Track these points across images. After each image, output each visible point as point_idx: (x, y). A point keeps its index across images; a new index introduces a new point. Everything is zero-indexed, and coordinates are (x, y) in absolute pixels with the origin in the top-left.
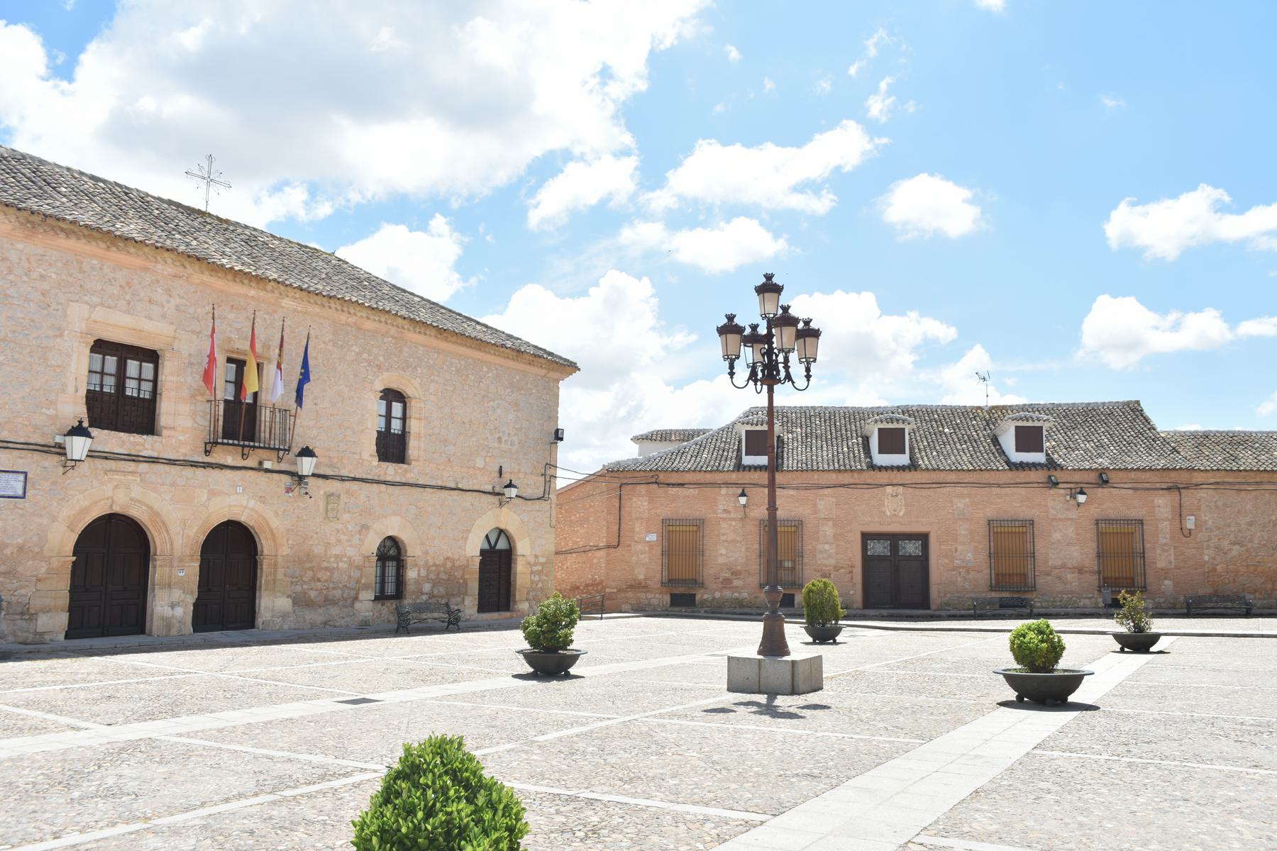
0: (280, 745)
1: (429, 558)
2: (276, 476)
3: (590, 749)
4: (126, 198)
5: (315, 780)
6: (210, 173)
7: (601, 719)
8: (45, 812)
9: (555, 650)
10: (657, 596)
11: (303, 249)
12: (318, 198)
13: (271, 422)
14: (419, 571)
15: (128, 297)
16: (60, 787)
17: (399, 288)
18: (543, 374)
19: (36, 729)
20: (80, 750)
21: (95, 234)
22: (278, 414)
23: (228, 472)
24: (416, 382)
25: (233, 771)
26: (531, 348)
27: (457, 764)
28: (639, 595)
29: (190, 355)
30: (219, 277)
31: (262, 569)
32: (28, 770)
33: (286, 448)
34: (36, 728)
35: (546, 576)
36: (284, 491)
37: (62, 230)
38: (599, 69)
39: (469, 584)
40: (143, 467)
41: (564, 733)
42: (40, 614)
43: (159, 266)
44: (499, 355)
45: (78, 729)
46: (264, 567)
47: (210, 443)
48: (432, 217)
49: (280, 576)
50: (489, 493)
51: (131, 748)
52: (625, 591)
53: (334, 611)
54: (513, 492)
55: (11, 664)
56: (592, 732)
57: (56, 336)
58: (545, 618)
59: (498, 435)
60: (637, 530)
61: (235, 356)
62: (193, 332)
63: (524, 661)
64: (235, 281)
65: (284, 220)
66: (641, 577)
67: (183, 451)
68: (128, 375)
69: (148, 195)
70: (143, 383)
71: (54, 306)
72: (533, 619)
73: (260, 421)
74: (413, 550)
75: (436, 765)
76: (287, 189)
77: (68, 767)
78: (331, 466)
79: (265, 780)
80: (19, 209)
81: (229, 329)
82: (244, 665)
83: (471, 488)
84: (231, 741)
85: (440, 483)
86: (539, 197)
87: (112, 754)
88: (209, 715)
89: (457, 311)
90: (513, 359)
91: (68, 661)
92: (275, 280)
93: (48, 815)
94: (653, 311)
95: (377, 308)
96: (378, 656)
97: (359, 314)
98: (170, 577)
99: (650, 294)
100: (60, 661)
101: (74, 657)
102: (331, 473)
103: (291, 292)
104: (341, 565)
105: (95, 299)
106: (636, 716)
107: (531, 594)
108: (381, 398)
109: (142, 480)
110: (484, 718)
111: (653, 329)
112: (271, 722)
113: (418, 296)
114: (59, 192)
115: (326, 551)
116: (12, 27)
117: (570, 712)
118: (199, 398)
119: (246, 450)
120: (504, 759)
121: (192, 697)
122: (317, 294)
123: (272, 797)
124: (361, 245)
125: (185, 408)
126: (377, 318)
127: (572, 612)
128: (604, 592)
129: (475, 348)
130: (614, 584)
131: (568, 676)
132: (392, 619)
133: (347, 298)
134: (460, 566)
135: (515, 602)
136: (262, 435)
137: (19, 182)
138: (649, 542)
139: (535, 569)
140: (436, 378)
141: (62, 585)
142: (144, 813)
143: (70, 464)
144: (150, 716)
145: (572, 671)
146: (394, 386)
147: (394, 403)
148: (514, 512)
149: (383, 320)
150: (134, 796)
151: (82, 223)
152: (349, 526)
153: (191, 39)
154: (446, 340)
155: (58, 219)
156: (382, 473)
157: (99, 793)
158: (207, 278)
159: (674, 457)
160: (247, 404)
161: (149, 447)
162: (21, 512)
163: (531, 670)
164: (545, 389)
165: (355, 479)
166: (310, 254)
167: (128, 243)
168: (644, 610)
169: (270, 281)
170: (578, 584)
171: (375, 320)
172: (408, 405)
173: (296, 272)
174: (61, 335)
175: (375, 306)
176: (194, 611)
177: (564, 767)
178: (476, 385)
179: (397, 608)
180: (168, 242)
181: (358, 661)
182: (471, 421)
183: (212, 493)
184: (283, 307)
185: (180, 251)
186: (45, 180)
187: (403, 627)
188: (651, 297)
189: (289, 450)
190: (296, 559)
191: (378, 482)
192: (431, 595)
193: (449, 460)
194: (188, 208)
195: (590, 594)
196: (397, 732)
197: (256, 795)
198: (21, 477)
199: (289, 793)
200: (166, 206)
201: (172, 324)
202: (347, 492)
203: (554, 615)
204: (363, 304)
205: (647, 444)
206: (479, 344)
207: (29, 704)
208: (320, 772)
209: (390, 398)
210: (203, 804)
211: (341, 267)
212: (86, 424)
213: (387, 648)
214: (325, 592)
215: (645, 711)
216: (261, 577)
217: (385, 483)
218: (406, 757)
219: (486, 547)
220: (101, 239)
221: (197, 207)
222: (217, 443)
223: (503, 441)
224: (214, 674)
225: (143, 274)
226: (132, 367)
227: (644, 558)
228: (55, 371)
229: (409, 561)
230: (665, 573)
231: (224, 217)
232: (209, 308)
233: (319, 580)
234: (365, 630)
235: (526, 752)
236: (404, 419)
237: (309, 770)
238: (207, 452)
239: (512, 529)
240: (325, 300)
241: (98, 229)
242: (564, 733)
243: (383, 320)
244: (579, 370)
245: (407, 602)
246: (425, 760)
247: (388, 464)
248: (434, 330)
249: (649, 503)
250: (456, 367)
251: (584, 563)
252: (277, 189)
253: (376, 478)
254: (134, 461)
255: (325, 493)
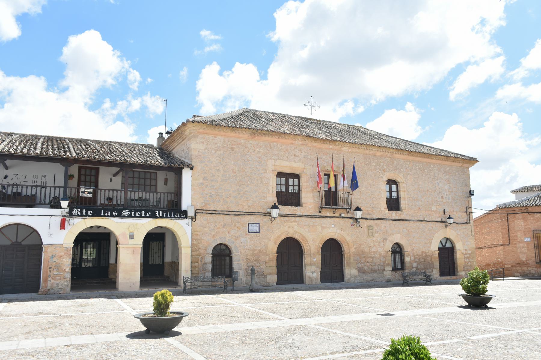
0: (354, 332)
1: (414, 252)
2: (346, 219)
3: (499, 345)
4: (284, 118)
5: (367, 348)
6: (312, 103)
7: (506, 331)
8: (267, 351)
9: (479, 295)
10: (534, 269)
11: (350, 126)
12: (358, 105)
13: (343, 198)
14: (410, 258)
15: (287, 155)
16: (273, 342)
17: (390, 136)
18: (460, 165)
19: (267, 319)
20: (280, 328)
21: (274, 133)
22: (345, 194)
23: (328, 219)
24: (401, 175)
25: (334, 341)
26: (453, 154)
27: (417, 350)
28: (524, 268)
29: (310, 174)
30: (318, 143)
31: (344, 257)
32: (263, 334)
33: (350, 208)
34: (266, 318)
35: (472, 259)
36: (350, 225)
37: (263, 134)
38: (479, 21)
39: (434, 263)
40: (298, 219)
41: (485, 336)
42: (268, 275)
43: (296, 142)
44: (438, 159)
45: (280, 320)
46: (345, 257)
47: (320, 208)
48: (406, 104)
49: (352, 260)
50: (440, 222)
51: (294, 330)
52: (515, 266)
53: (375, 275)
54: (451, 221)
55: (259, 294)
56: (500, 336)
57: (264, 173)
58: (472, 279)
59: (441, 195)
60: (519, 236)
61: (327, 173)
62: (311, 165)
63: (463, 300)
64: (324, 143)
65: (345, 116)
66: (524, 259)
67: (311, 212)
68: (289, 184)
69: (291, 116)
70: (295, 187)
71: (263, 162)
72: (466, 280)
73: (339, 198)
74: (407, 249)
75: (406, 350)
76: (345, 104)
77: (276, 334)
78: (368, 214)
79: (347, 346)
80: (249, 129)
81: (324, 162)
82: (340, 297)
83: (431, 220)
84: (334, 329)
85: (416, 219)
86: (455, 85)
87: (291, 330)
88: (326, 317)
89: (417, 143)
90: (445, 160)
91: (277, 293)
92: (339, 140)
93: (268, 353)
94: (520, 129)
95: (381, 146)
96: (395, 295)
97: (374, 150)
98: (310, 261)
99: (518, 121)
100: (275, 293)
101: (279, 292)
102: (369, 217)
103: (346, 144)
104: (376, 255)
105: (276, 157)
106: (525, 330)
107: (466, 268)
108: (387, 184)
109: (297, 224)
110: (444, 326)
111: (521, 137)
112: (350, 322)
113: (399, 139)
114: (262, 121)
115: (369, 250)
116: (248, 65)
117: (488, 326)
118: (315, 191)
119: (334, 210)
120: (454, 346)
121: (320, 309)
122: (356, 144)
123: (349, 354)
124: (377, 121)
125: (310, 195)
126: (382, 150)
127: (486, 276)
128: (504, 267)
129: (426, 157)
130: (509, 263)
131: (487, 308)
132: (400, 278)
133: (368, 144)
134: (429, 255)
135: (458, 272)
136: (340, 203)
137: (249, 119)
138: (526, 242)
139: (466, 256)
140: (410, 173)
141: (274, 264)
142: (301, 355)
143: (273, 219)
144: (305, 316)
145: (489, 305)
146: (392, 178)
147: (392, 185)
148: (453, 230)
149: (384, 150)
150: (298, 348)
151: (269, 130)
152: (378, 239)
153: (304, 54)
154: (413, 155)
155: (262, 130)
156: (390, 215)
157: (286, 346)
158: (314, 144)
159: (536, 199)
160: (333, 191)
161: (299, 211)
162: (258, 238)
163: (467, 304)
164: (462, 172)
165: (379, 219)
166: (352, 128)
167: (285, 135)
168: (528, 276)
169: (337, 141)
170: (490, 263)
171: (381, 151)
172: (398, 186)
173: (347, 136)
174: (266, 172)
175: (380, 145)
176: (320, 274)
177: (485, 353)
178: (429, 174)
179: (402, 274)
180: (299, 132)
181: (387, 297)
182: (428, 190)
183: (323, 228)
184: (343, 151)
185: (303, 134)
186: (257, 117)
187: (406, 283)
188: (518, 123)
189: (351, 209)
190: (358, 253)
191: (389, 220)
192: (417, 268)
193: (420, 208)
194: (305, 118)
195: (497, 268)
196: (403, 330)
197: (343, 352)
198: (258, 225)
199: (356, 353)
200: (298, 119)
201: (303, 163)
202: (376, 224)
203: (476, 278)
204: (375, 145)
205: (520, 194)
206: (428, 155)
207: (265, 309)
208: (370, 345)
209: (391, 183)
210: (323, 354)
211: (365, 131)
212: (277, 204)
213: (399, 292)
214: (371, 267)
215: (530, 328)
216: (345, 261)
217: (392, 220)
218: (392, 345)
219: (441, 246)
220: (276, 135)
221: (308, 117)
222: (323, 208)
223: (444, 198)
224: (329, 300)
225: (291, 145)
226: (291, 180)
227: (525, 250)
228: (265, 185)
229: (406, 254)
230: (538, 257)
231: (318, 119)
232: (315, 155)
233: (368, 262)
234: (389, 284)
235: (466, 344)
236: (397, 192)
237: (365, 344)
238: (320, 212)
239: (452, 238)
240: (359, 145)
241: (275, 132)
242: (485, 336)
243: (384, 150)
244: (479, 161)
245: (407, 271)
246: (401, 347)
247: (392, 211)
248: (407, 152)
249: (524, 223)
250: (418, 167)
251: (492, 253)
252: (341, 104)
253: (388, 218)
254: (294, 217)
255: (367, 226)
